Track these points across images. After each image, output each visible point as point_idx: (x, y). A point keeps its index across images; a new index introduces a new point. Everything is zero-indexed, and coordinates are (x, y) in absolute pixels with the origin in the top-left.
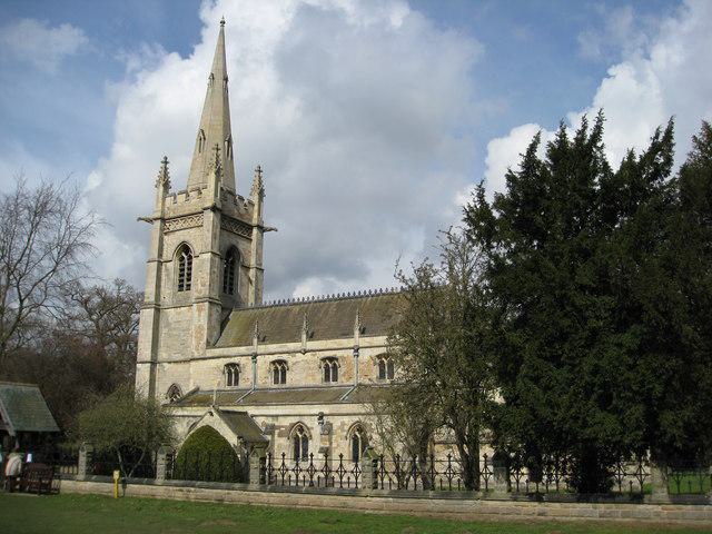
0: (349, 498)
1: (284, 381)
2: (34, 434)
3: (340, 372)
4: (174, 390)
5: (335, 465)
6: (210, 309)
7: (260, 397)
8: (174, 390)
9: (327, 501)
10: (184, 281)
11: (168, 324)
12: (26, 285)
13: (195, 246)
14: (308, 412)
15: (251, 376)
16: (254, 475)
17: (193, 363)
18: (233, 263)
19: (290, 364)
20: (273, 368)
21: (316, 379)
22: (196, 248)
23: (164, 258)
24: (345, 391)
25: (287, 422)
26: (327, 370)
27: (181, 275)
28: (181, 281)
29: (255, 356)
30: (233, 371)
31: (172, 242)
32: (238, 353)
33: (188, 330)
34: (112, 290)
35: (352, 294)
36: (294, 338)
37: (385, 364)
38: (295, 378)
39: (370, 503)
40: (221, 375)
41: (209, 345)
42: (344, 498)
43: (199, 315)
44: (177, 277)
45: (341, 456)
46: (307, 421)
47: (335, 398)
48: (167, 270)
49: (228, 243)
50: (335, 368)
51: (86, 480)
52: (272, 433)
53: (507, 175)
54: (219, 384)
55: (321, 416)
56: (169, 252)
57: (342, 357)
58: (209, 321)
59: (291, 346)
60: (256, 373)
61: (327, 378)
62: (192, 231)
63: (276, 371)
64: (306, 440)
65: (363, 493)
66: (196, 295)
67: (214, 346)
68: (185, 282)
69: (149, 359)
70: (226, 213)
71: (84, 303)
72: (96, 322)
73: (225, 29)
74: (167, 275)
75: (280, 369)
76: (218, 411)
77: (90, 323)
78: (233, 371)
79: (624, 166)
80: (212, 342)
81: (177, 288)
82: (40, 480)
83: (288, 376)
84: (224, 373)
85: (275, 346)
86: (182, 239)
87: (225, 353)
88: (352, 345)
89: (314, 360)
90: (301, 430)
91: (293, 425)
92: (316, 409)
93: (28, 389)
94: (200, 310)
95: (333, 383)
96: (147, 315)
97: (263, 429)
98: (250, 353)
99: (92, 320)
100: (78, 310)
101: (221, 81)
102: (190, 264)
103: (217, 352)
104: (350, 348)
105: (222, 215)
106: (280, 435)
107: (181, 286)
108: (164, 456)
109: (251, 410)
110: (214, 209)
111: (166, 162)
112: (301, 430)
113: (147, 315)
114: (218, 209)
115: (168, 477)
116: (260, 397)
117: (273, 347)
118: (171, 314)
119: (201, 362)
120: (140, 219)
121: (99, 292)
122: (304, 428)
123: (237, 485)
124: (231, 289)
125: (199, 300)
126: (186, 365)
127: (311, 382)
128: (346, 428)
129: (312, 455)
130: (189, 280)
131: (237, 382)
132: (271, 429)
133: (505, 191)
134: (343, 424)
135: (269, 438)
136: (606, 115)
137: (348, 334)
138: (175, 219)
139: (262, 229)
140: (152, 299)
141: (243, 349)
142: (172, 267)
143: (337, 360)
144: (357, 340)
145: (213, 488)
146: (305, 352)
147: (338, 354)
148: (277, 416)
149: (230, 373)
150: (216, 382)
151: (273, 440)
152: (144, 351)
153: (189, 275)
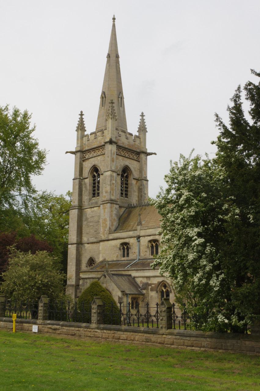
0: (152, 335)
4: (91, 261)
6: (111, 207)
8: (91, 261)
10: (95, 191)
11: (87, 219)
13: (101, 167)
15: (137, 251)
17: (101, 243)
18: (127, 177)
20: (150, 245)
21: (146, 253)
22: (102, 169)
25: (155, 281)
27: (94, 187)
28: (94, 191)
29: (139, 237)
30: (125, 247)
31: (87, 166)
33: (98, 222)
40: (118, 251)
43: (104, 212)
44: (91, 188)
48: (85, 184)
49: (122, 164)
50: (128, 249)
53: (229, 117)
54: (117, 257)
58: (111, 216)
62: (99, 158)
68: (96, 192)
70: (121, 145)
73: (116, 23)
76: (109, 275)
78: (125, 247)
81: (92, 195)
84: (120, 249)
86: (93, 164)
90: (165, 286)
91: (160, 283)
94: (104, 209)
96: (74, 214)
97: (141, 285)
98: (135, 235)
101: (115, 58)
104: (135, 237)
105: (117, 145)
106: (152, 290)
107: (94, 194)
109: (134, 274)
111: (82, 115)
112: (165, 286)
113: (74, 214)
116: (143, 265)
118: (88, 212)
119: (106, 243)
120: (67, 152)
122: (167, 285)
123: (84, 325)
124: (126, 195)
125: (104, 203)
126: (98, 245)
130: (98, 190)
133: (231, 127)
135: (144, 292)
138: (89, 151)
141: (131, 233)
142: (88, 181)
145: (70, 326)
149: (124, 249)
150: (115, 255)
152: (73, 237)
153: (98, 187)
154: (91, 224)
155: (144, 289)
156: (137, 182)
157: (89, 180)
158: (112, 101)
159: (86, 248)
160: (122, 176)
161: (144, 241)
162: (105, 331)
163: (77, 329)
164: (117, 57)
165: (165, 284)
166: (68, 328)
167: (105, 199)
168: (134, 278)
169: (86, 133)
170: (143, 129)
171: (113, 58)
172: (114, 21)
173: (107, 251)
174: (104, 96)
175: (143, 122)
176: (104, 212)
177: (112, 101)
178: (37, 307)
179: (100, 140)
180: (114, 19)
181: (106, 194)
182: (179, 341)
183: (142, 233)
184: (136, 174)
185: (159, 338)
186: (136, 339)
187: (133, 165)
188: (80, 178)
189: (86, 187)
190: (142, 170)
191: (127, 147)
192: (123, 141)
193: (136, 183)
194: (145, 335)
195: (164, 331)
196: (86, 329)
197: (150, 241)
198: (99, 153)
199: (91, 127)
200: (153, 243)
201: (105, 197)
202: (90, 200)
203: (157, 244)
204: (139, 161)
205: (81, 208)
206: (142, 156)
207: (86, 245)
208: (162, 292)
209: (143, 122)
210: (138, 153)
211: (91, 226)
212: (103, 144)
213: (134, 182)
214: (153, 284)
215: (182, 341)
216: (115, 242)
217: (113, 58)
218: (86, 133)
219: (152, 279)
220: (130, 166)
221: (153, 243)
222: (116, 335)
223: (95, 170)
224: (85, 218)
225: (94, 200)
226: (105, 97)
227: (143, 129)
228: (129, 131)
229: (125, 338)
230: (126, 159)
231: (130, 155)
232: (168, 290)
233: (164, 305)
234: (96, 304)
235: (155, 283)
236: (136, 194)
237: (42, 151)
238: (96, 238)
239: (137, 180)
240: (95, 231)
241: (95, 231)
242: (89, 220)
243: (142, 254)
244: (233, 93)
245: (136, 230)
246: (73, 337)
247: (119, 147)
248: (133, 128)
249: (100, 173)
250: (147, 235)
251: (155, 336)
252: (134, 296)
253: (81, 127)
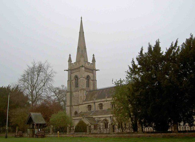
1: (102, 109)
2: (41, 124)
4: (76, 113)
7: (96, 113)
8: (76, 113)
10: (77, 85)
12: (37, 90)
16: (88, 131)
18: (89, 79)
19: (103, 104)
22: (79, 77)
25: (102, 119)
28: (76, 85)
29: (95, 103)
30: (90, 107)
31: (73, 75)
32: (90, 102)
34: (61, 88)
36: (104, 98)
37: (113, 104)
44: (75, 84)
46: (107, 119)
48: (72, 82)
55: (110, 117)
56: (73, 78)
59: (103, 100)
60: (95, 107)
63: (100, 106)
64: (107, 123)
67: (85, 101)
69: (69, 105)
71: (54, 92)
72: (58, 96)
75: (101, 106)
77: (56, 97)
78: (90, 107)
79: (170, 51)
83: (103, 108)
85: (103, 99)
87: (88, 102)
90: (106, 121)
91: (104, 120)
92: (109, 116)
93: (40, 114)
94: (81, 92)
96: (69, 94)
99: (56, 96)
100: (53, 94)
103: (86, 102)
106: (101, 122)
107: (76, 86)
112: (106, 121)
116: (96, 113)
117: (99, 100)
121: (58, 89)
131: (91, 110)
132: (98, 121)
136: (143, 48)
141: (92, 101)
142: (74, 81)
145: (79, 134)
153: (78, 84)
155: (98, 122)
157: (74, 80)
158: (82, 49)
161: (97, 104)
164: (83, 33)
168: (94, 118)
169: (72, 63)
170: (94, 60)
171: (82, 33)
172: (81, 19)
173: (83, 109)
175: (94, 58)
177: (82, 49)
179: (78, 66)
180: (81, 18)
183: (96, 101)
184: (92, 79)
185: (111, 135)
187: (91, 75)
188: (70, 81)
195: (112, 133)
197: (99, 104)
199: (74, 60)
205: (71, 92)
206: (94, 71)
209: (94, 58)
210: (93, 70)
216: (85, 105)
217: (82, 33)
218: (72, 63)
219: (101, 118)
223: (76, 77)
227: (94, 60)
228: (89, 61)
236: (92, 86)
237: (46, 65)
239: (92, 80)
243: (96, 109)
244: (131, 61)
245: (94, 100)
246: (81, 138)
247: (85, 68)
248: (90, 60)
251: (109, 135)
253: (70, 60)
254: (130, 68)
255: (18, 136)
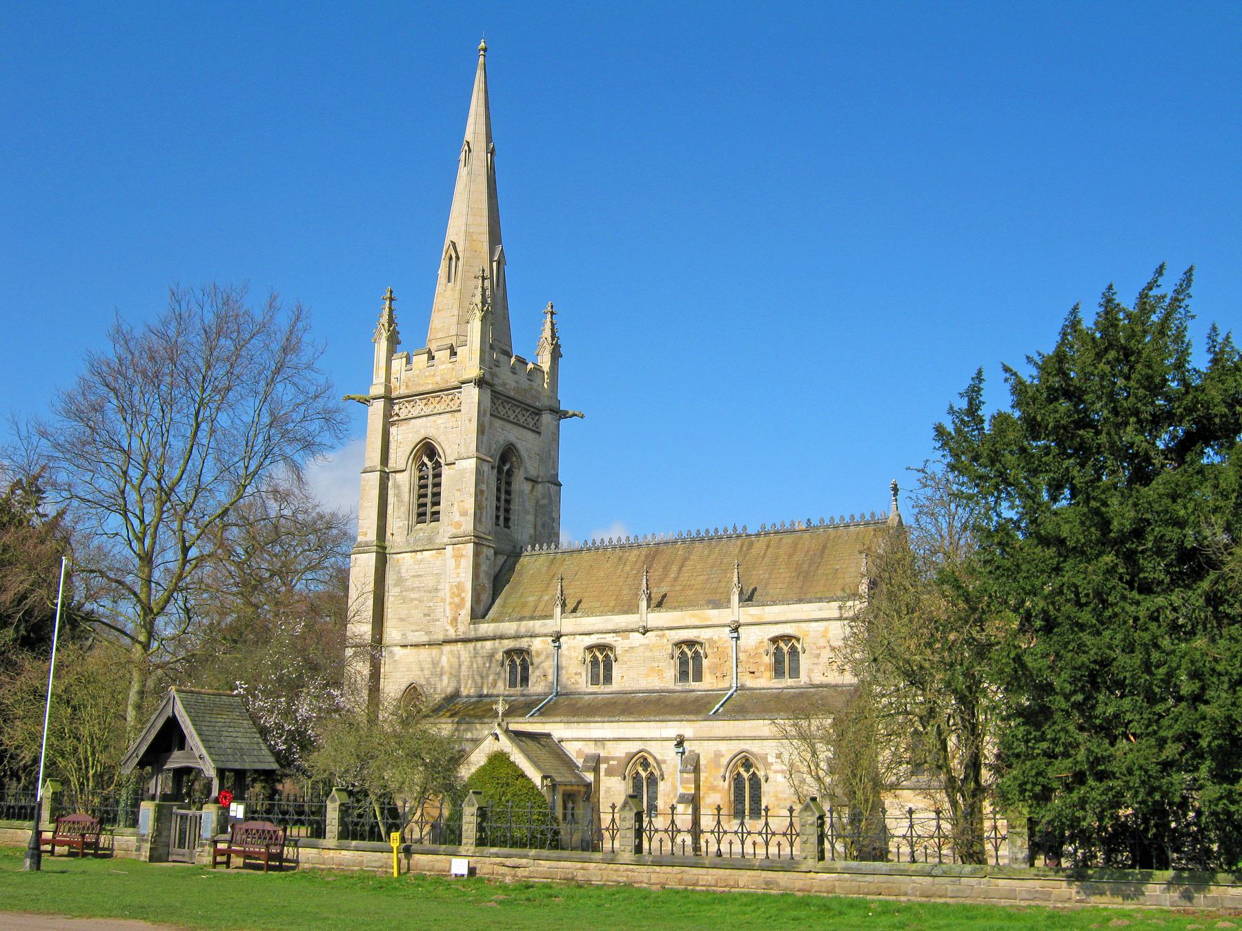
1: (608, 679)
3: (804, 661)
5: (707, 822)
9: (706, 877)
10: (427, 506)
11: (400, 581)
14: (655, 737)
18: (509, 473)
19: (619, 651)
20: (589, 658)
21: (665, 678)
23: (392, 464)
24: (718, 697)
25: (620, 751)
26: (683, 662)
29: (557, 637)
31: (404, 439)
35: (703, 533)
38: (625, 678)
39: (821, 881)
41: (478, 615)
42: (721, 872)
43: (458, 566)
45: (613, 807)
46: (656, 750)
47: (696, 707)
48: (397, 486)
50: (697, 657)
51: (340, 848)
52: (596, 770)
56: (400, 454)
57: (710, 640)
61: (683, 675)
62: (440, 420)
63: (595, 662)
64: (653, 781)
65: (804, 868)
66: (453, 531)
68: (429, 509)
70: (500, 389)
74: (398, 495)
75: (602, 660)
76: (507, 731)
80: (482, 608)
82: (267, 846)
84: (502, 665)
88: (728, 621)
89: (662, 645)
90: (645, 764)
92: (672, 729)
94: (458, 557)
95: (790, 682)
97: (580, 762)
102: (438, 475)
104: (546, 635)
106: (609, 773)
107: (421, 515)
108: (474, 810)
110: (480, 383)
114: (488, 384)
115: (481, 842)
118: (404, 564)
122: (651, 760)
124: (507, 520)
125: (456, 540)
127: (655, 683)
128: (725, 761)
129: (767, 809)
132: (595, 763)
134: (718, 755)
135: (590, 777)
137: (719, 602)
139: (561, 415)
140: (372, 536)
142: (404, 482)
143: (701, 644)
144: (736, 612)
146: (646, 631)
147: (703, 635)
148: (603, 740)
149: (513, 665)
151: (597, 780)
152: (361, 629)
154: (413, 595)
156: (533, 487)
159: (397, 658)
160: (500, 471)
161: (574, 649)
162: (657, 869)
163: (579, 865)
165: (645, 759)
166: (554, 864)
167: (460, 531)
174: (454, 256)
176: (458, 566)
178: (321, 811)
181: (462, 519)
182: (848, 884)
184: (531, 466)
186: (741, 884)
187: (525, 442)
189: (398, 495)
190: (550, 456)
191: (512, 394)
192: (507, 381)
193: (532, 491)
194: (764, 874)
196: (604, 866)
197: (590, 648)
198: (441, 407)
200: (598, 654)
201: (459, 525)
202: (410, 529)
203: (607, 656)
204: (539, 433)
207: (397, 649)
208: (637, 778)
211: (413, 600)
212: (456, 383)
213: (527, 487)
214: (613, 758)
215: (854, 883)
220: (519, 446)
221: (598, 654)
222: (686, 877)
223: (428, 449)
224: (395, 577)
225: (425, 528)
226: (457, 258)
229: (713, 883)
230: (509, 426)
231: (520, 416)
232: (652, 773)
233: (811, 810)
234: (631, 809)
235: (617, 755)
238: (428, 633)
239: (533, 481)
240: (425, 615)
241: (425, 615)
242: (408, 583)
245: (550, 616)
247: (496, 395)
249: (442, 461)
250: (581, 631)
252: (569, 788)
254: (1109, 307)
255: (62, 844)
